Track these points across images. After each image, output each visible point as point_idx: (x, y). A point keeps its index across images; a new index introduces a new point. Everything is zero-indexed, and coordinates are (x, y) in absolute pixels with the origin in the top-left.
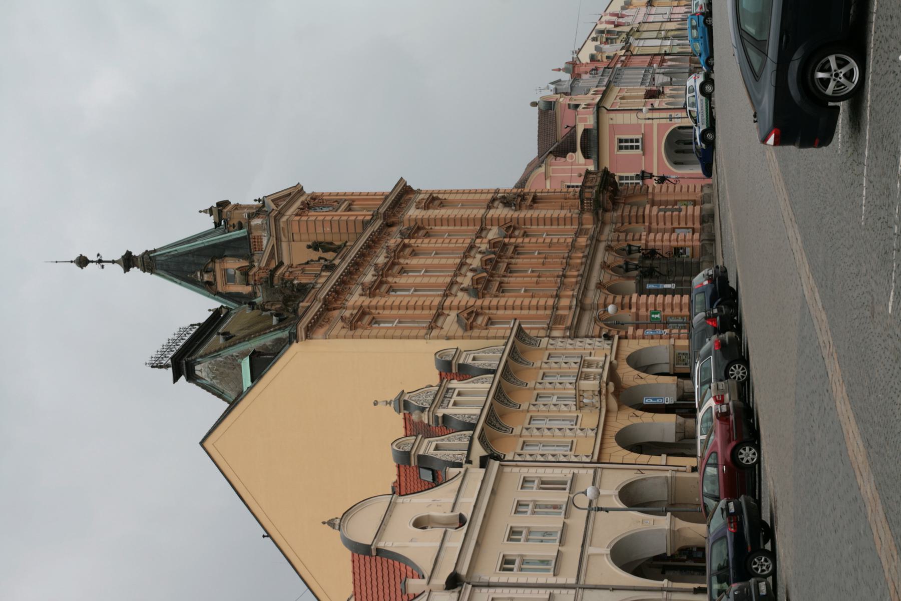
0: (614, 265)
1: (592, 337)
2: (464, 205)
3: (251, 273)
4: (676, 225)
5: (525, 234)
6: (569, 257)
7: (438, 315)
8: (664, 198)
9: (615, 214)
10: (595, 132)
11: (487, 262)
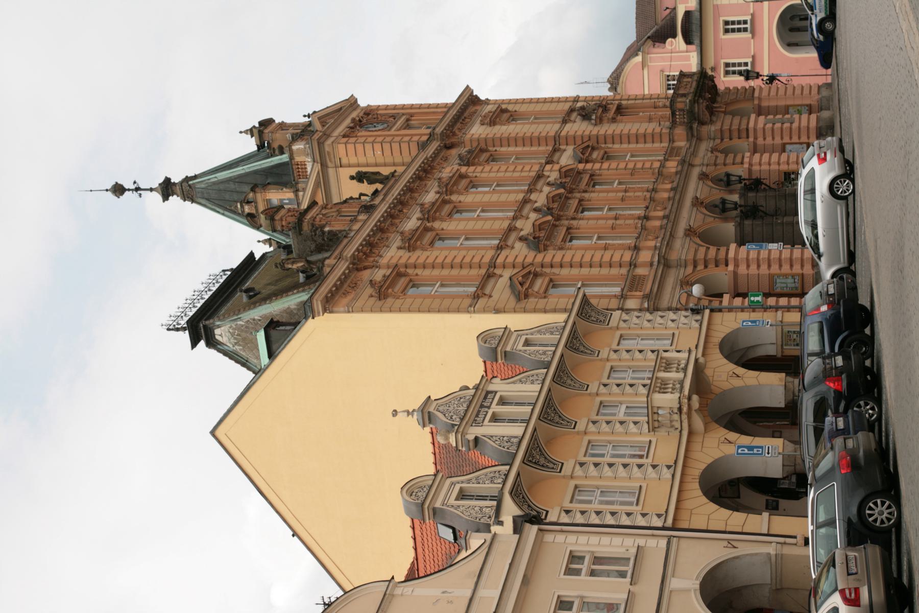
0: (707, 201)
1: (677, 309)
2: (538, 117)
3: (277, 217)
4: (786, 139)
5: (607, 157)
6: (654, 190)
7: (489, 276)
8: (773, 103)
9: (713, 128)
10: (697, 14)
11: (553, 199)
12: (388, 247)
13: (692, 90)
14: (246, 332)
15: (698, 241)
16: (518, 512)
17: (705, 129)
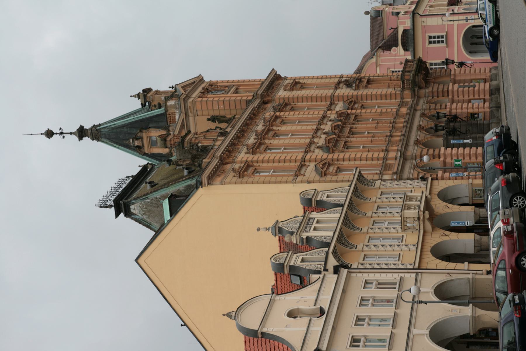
2: (319, 87)
3: (168, 139)
4: (471, 97)
5: (363, 107)
6: (394, 122)
7: (301, 166)
8: (463, 78)
9: (427, 91)
10: (411, 32)
11: (335, 127)
12: (239, 152)
13: (414, 69)
14: (151, 206)
15: (422, 146)
16: (336, 264)
17: (422, 91)
